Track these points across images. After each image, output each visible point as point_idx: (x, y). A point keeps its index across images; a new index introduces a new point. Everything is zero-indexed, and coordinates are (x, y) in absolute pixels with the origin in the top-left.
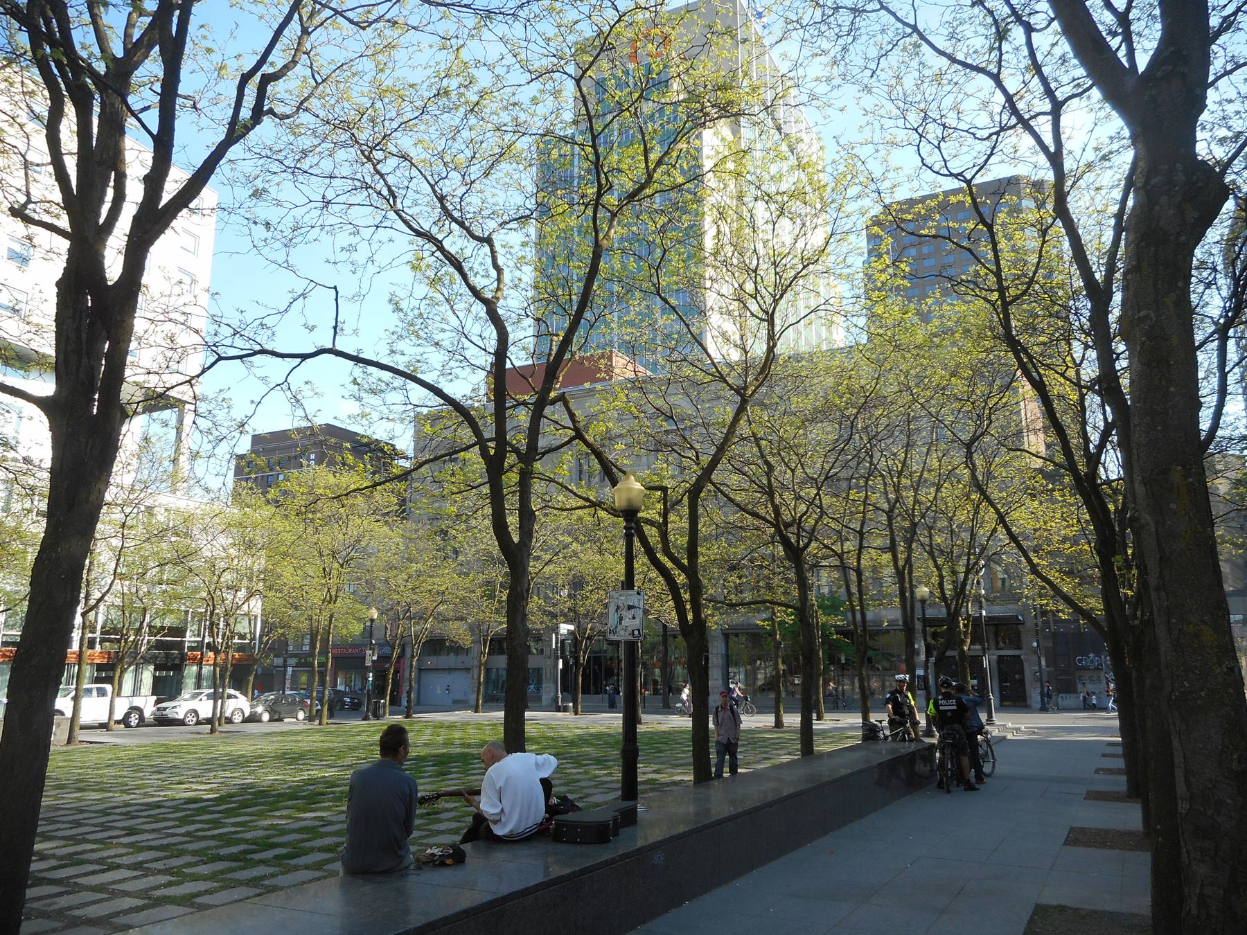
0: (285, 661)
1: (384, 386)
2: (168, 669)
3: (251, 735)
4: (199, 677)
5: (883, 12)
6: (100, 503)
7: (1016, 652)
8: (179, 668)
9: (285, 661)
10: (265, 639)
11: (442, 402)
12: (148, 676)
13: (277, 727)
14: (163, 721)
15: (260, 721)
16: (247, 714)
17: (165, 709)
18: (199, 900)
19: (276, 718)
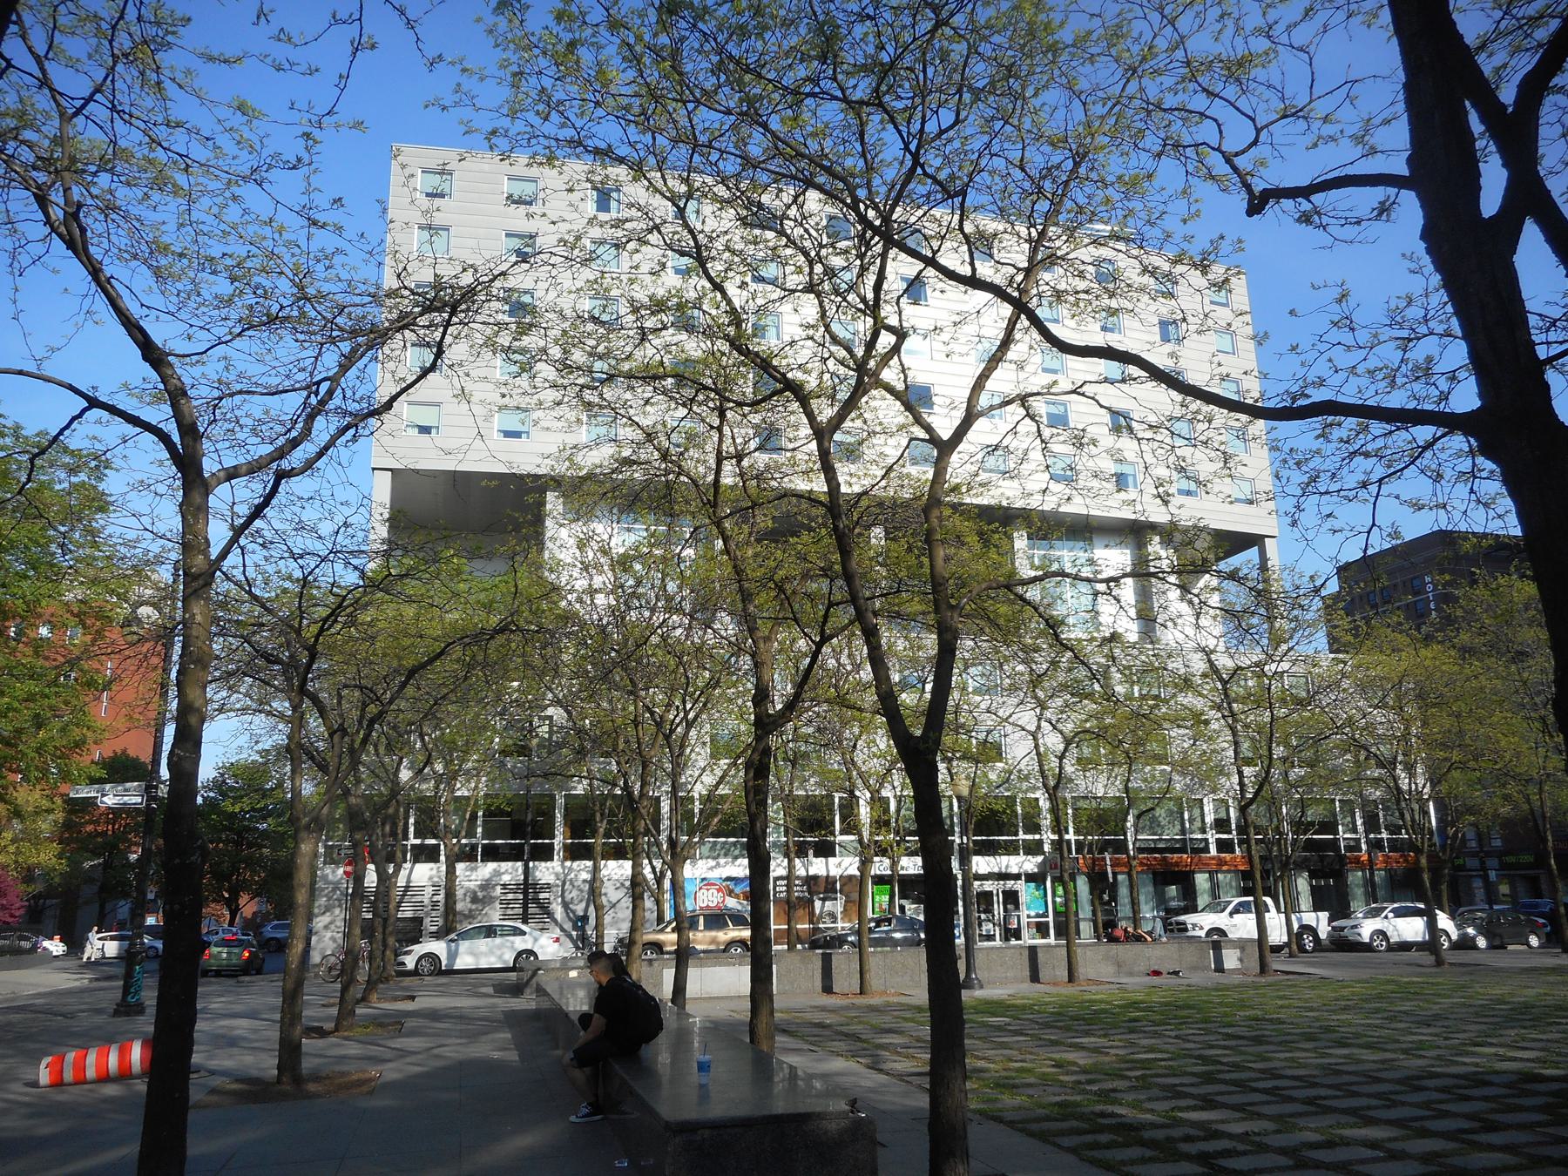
0: (1482, 863)
1: (1180, 87)
2: (1326, 877)
3: (1497, 971)
4: (1370, 884)
5: (96, 413)
6: (1438, 269)
7: (1037, 837)
8: (1340, 875)
9: (1482, 863)
10: (1451, 831)
11: (1049, 325)
12: (1303, 884)
13: (1499, 960)
14: (1343, 944)
15: (1475, 947)
16: (1454, 937)
17: (1342, 929)
18: (1476, 1125)
19: (1496, 945)
